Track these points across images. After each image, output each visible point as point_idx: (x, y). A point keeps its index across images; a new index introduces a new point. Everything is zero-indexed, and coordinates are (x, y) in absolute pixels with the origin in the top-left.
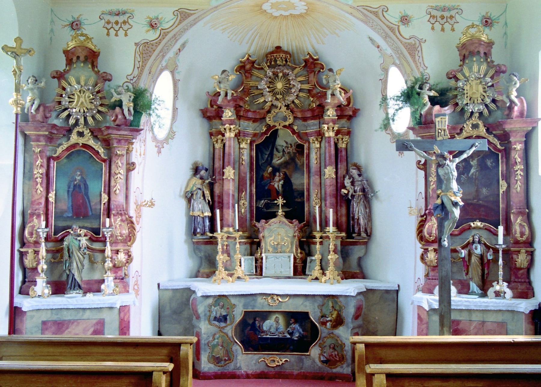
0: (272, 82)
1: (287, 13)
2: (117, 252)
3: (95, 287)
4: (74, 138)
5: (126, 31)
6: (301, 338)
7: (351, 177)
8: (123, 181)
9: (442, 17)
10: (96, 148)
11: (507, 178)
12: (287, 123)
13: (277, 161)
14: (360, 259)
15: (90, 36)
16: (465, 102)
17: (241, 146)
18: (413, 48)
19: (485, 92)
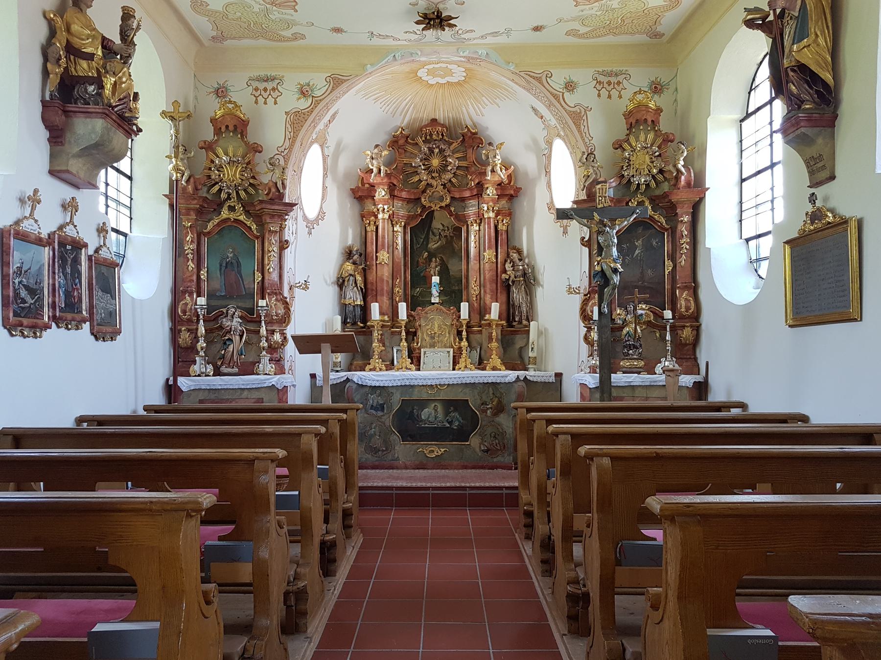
0: (426, 159)
1: (443, 81)
2: (273, 332)
3: (248, 369)
4: (225, 213)
5: (275, 99)
6: (461, 427)
7: (512, 261)
8: (277, 259)
9: (609, 83)
10: (248, 223)
11: (673, 258)
12: (443, 204)
13: (433, 246)
14: (521, 348)
15: (239, 103)
16: (631, 174)
17: (395, 229)
18: (578, 117)
19: (652, 162)
